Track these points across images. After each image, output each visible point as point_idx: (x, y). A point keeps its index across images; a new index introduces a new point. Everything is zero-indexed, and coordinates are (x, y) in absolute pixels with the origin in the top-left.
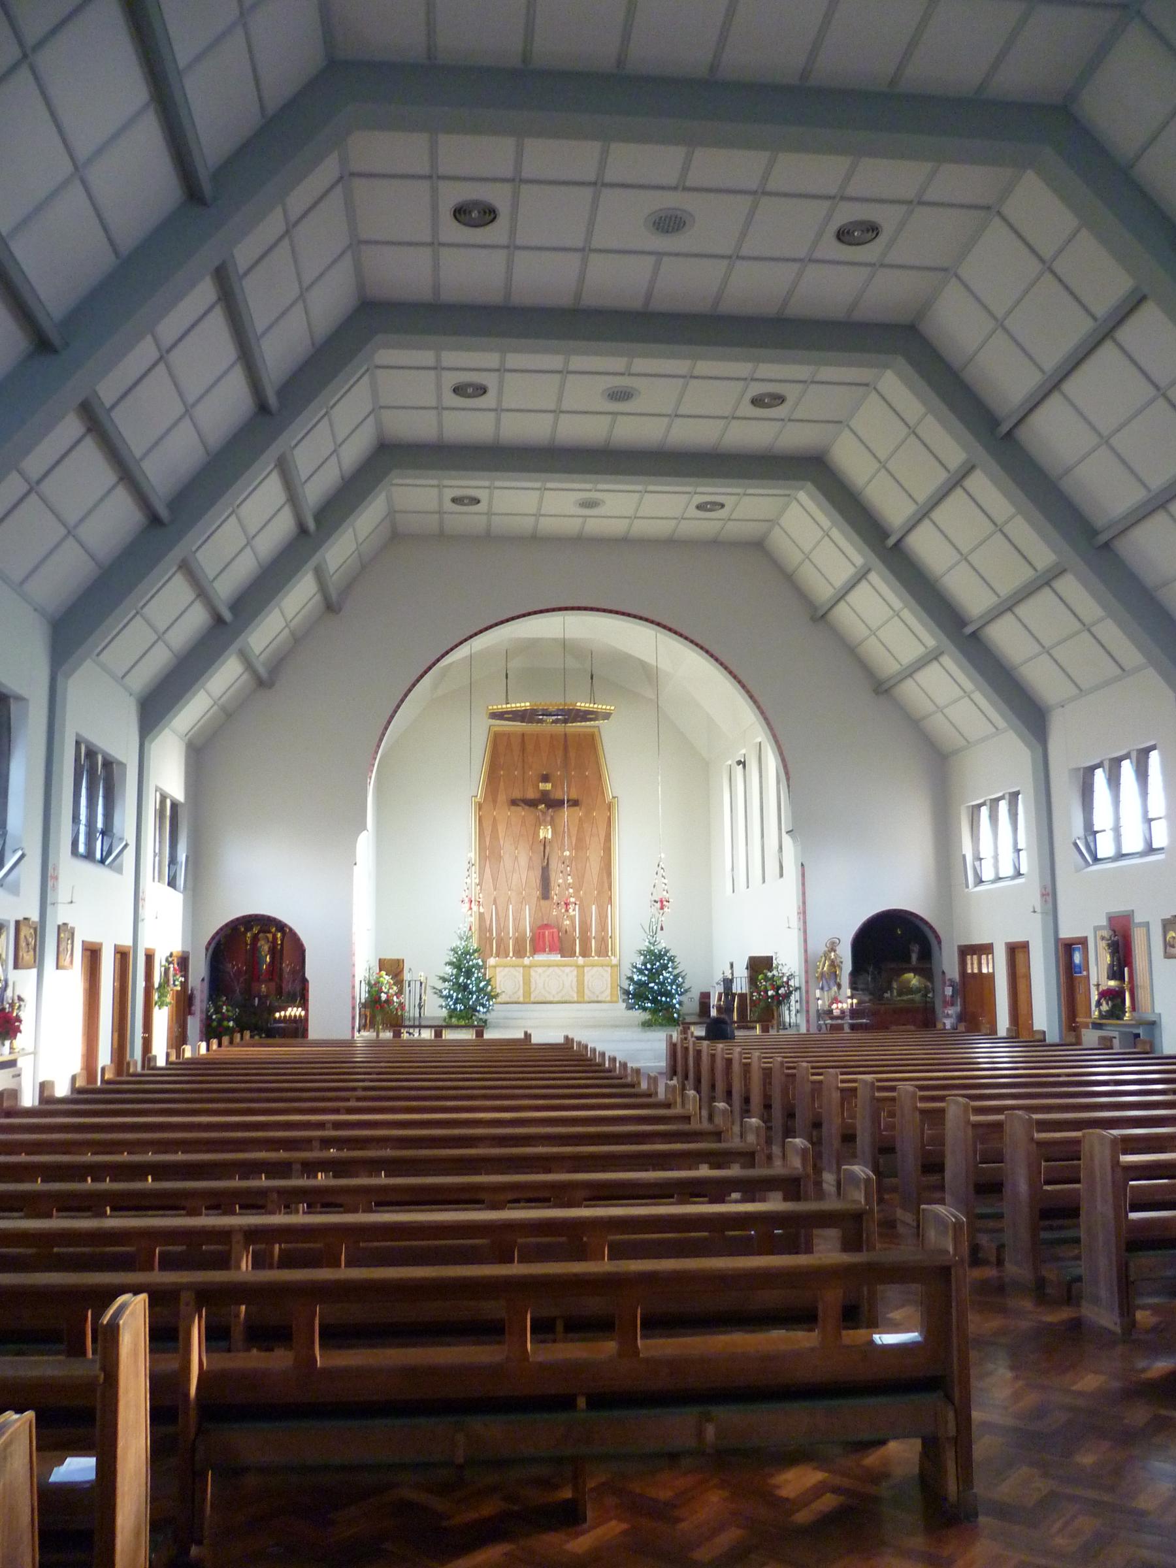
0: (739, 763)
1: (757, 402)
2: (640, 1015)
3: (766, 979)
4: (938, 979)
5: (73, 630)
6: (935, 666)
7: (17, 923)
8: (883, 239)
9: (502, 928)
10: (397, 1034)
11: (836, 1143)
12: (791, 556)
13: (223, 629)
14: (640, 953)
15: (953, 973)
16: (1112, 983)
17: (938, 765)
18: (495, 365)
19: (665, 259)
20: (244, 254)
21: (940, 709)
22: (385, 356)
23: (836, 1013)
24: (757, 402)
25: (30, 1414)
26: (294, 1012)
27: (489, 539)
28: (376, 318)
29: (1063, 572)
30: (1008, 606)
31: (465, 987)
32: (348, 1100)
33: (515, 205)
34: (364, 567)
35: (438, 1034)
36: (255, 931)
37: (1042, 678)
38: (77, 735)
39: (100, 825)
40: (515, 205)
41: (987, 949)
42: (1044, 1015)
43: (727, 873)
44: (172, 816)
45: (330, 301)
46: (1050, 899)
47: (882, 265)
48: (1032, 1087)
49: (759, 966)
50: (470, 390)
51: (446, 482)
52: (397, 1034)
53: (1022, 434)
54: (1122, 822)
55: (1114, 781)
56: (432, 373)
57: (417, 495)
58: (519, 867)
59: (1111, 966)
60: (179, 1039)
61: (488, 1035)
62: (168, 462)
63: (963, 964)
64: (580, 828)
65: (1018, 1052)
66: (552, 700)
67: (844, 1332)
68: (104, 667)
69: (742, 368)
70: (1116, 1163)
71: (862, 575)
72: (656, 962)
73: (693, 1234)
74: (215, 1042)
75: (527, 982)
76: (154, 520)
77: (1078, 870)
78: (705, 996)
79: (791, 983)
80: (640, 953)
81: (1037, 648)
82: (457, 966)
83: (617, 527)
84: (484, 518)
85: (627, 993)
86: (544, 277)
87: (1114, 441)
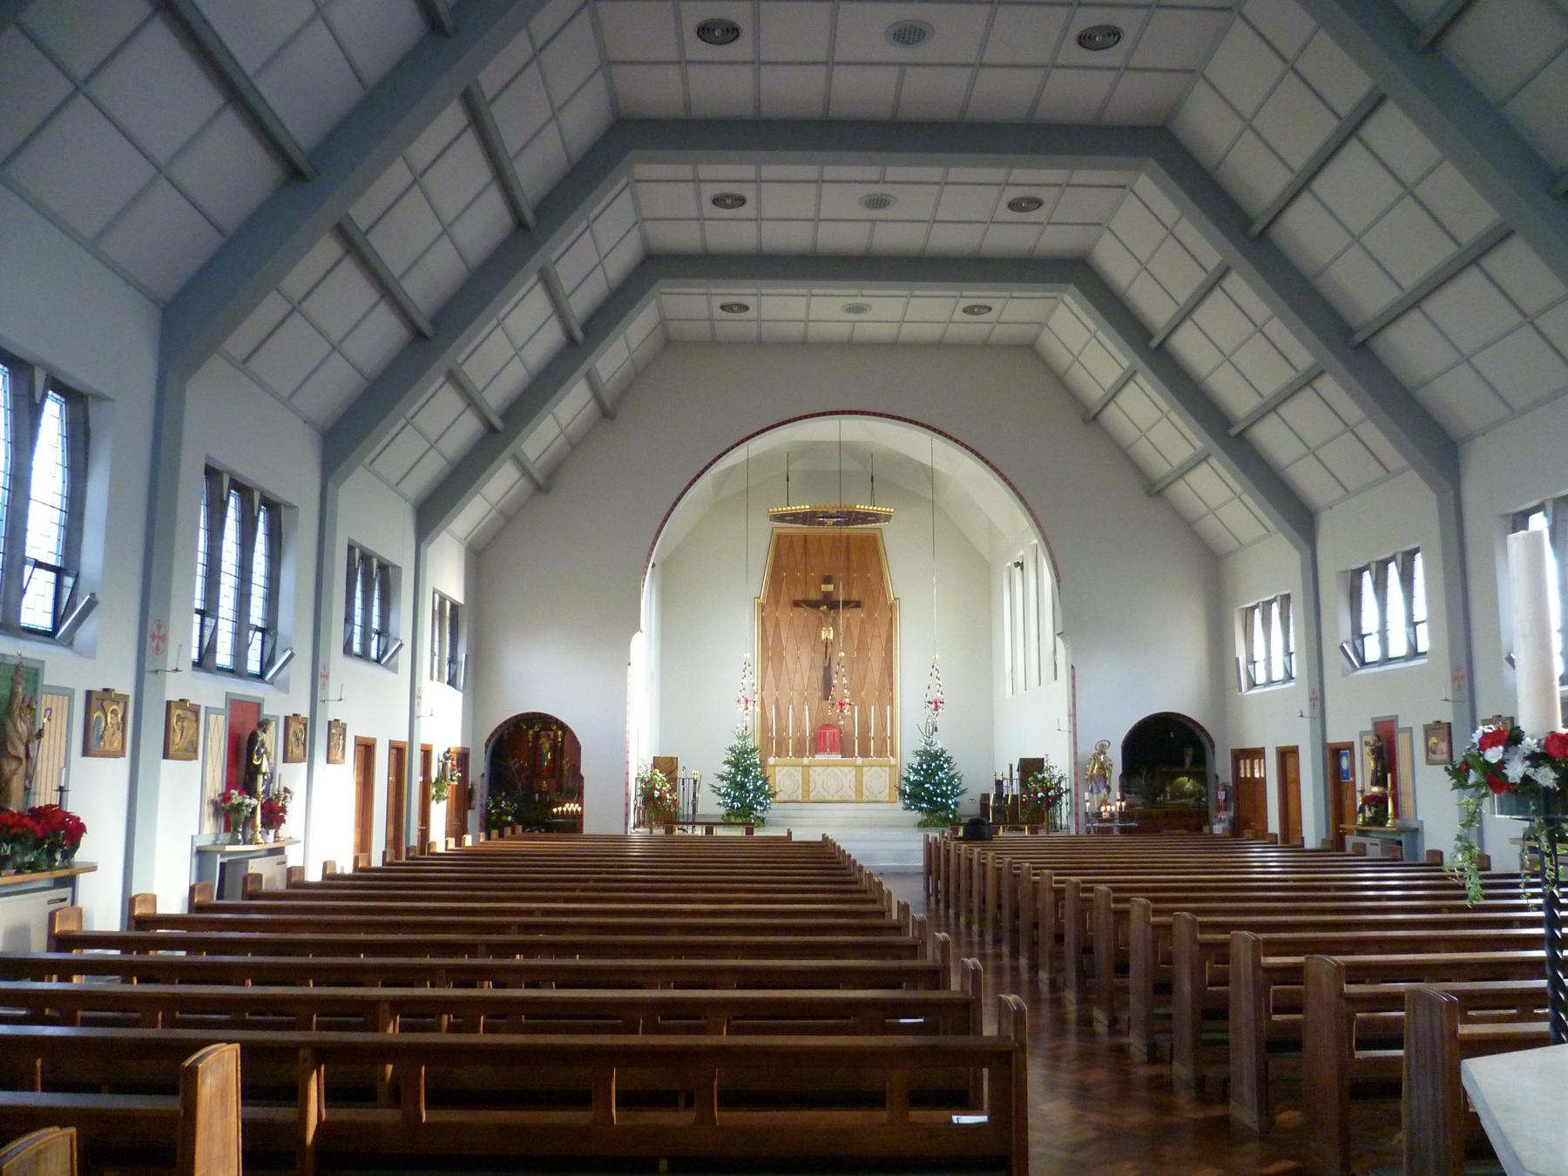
0: (1017, 564)
1: (1014, 206)
2: (916, 816)
3: (1036, 781)
4: (1210, 780)
5: (343, 440)
6: (1204, 467)
7: (287, 718)
8: (1125, 44)
9: (782, 729)
10: (670, 831)
11: (1050, 942)
12: (1061, 359)
13: (495, 437)
14: (917, 753)
15: (1226, 776)
16: (1376, 789)
17: (1213, 571)
18: (752, 176)
19: (909, 70)
20: (489, 80)
21: (1212, 511)
22: (641, 170)
23: (1106, 816)
24: (1014, 206)
25: (73, 1130)
26: (571, 807)
27: (761, 345)
28: (629, 135)
29: (1322, 372)
30: (1272, 407)
31: (742, 786)
32: (573, 890)
33: (756, 18)
34: (637, 376)
35: (709, 831)
36: (537, 728)
37: (1308, 479)
38: (208, 457)
39: (375, 625)
40: (756, 18)
41: (1258, 753)
42: (1312, 832)
43: (1009, 677)
44: (451, 617)
45: (584, 119)
46: (1318, 704)
47: (1127, 69)
48: (1303, 892)
49: (1030, 767)
50: (729, 201)
51: (714, 291)
52: (670, 831)
53: (1277, 233)
54: (1389, 626)
55: (1381, 587)
56: (691, 185)
57: (689, 304)
58: (801, 668)
59: (1375, 772)
60: (457, 829)
61: (757, 833)
62: (429, 278)
63: (1236, 769)
64: (862, 630)
65: (1289, 857)
66: (830, 504)
67: (912, 1113)
68: (376, 475)
69: (998, 174)
70: (1257, 964)
71: (1128, 378)
72: (933, 762)
73: (161, 952)
74: (495, 833)
75: (806, 782)
76: (418, 335)
77: (1345, 674)
78: (985, 797)
79: (1063, 785)
80: (917, 753)
81: (1303, 450)
82: (735, 765)
83: (886, 331)
84: (754, 324)
85: (902, 793)
86: (793, 90)
87: (1364, 240)
